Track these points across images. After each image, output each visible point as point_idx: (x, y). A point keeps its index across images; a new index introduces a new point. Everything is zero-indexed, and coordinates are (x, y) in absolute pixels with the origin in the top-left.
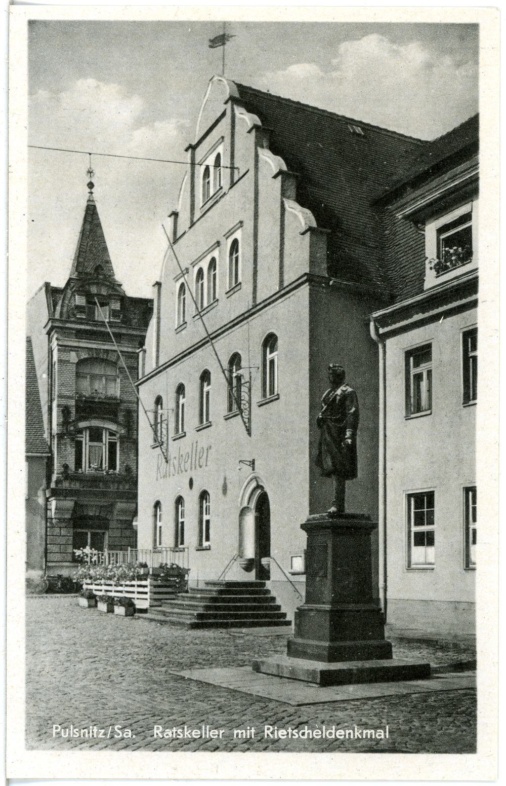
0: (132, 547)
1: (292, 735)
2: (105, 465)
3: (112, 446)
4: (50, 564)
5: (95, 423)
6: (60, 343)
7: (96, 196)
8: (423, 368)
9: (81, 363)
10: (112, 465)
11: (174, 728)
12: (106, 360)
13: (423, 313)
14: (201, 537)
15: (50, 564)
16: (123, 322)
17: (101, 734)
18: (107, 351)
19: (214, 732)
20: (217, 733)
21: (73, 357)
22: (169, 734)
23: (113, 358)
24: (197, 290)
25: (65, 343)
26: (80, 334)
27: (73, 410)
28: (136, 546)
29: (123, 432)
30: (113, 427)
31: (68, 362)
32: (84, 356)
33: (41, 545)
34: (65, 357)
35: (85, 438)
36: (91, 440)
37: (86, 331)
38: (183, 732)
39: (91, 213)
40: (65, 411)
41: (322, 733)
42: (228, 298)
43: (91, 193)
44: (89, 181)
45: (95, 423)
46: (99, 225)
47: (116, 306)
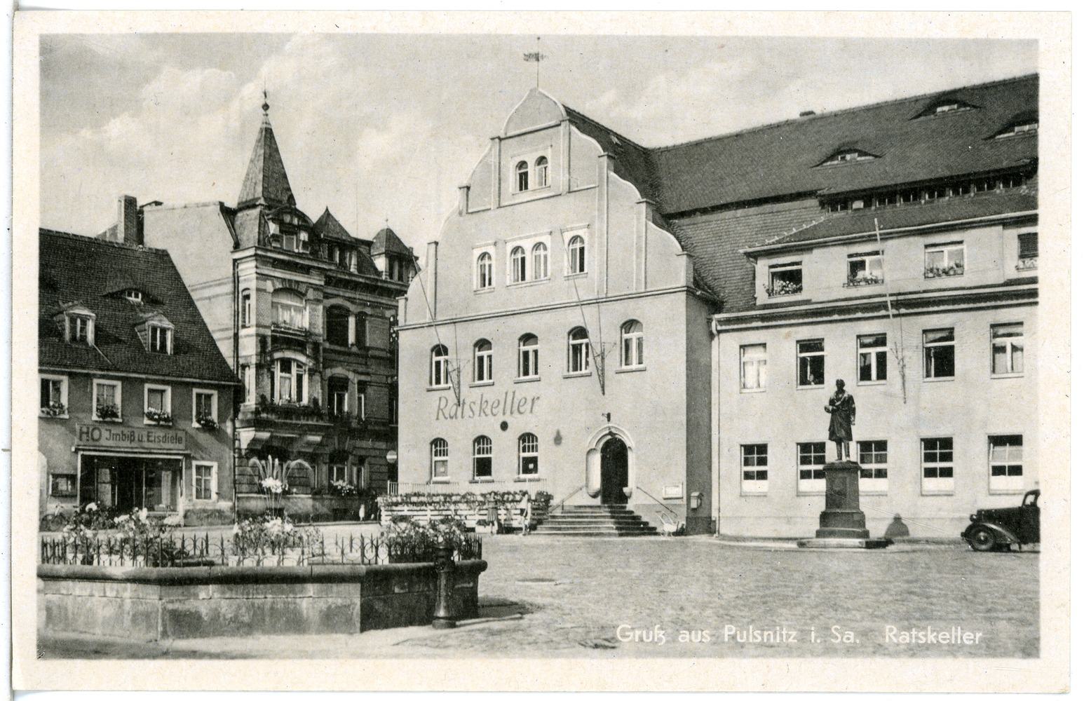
0: (392, 480)
1: (917, 638)
2: (294, 397)
3: (300, 378)
4: (240, 495)
5: (288, 354)
6: (259, 271)
7: (271, 119)
8: (633, 335)
9: (277, 292)
10: (300, 398)
11: (914, 630)
12: (297, 291)
13: (863, 313)
14: (431, 473)
15: (240, 495)
16: (311, 254)
17: (792, 637)
18: (297, 282)
19: (945, 635)
20: (972, 637)
21: (269, 286)
22: (905, 638)
23: (302, 289)
24: (638, 265)
25: (266, 272)
26: (277, 264)
27: (269, 340)
28: (397, 481)
29: (311, 364)
30: (302, 358)
31: (265, 291)
32: (279, 286)
33: (230, 476)
34: (262, 285)
35: (277, 369)
36: (282, 371)
37: (282, 261)
38: (926, 636)
39: (268, 135)
40: (262, 340)
41: (951, 635)
42: (1021, 324)
43: (267, 115)
44: (264, 103)
45: (288, 354)
46: (277, 150)
47: (304, 236)
